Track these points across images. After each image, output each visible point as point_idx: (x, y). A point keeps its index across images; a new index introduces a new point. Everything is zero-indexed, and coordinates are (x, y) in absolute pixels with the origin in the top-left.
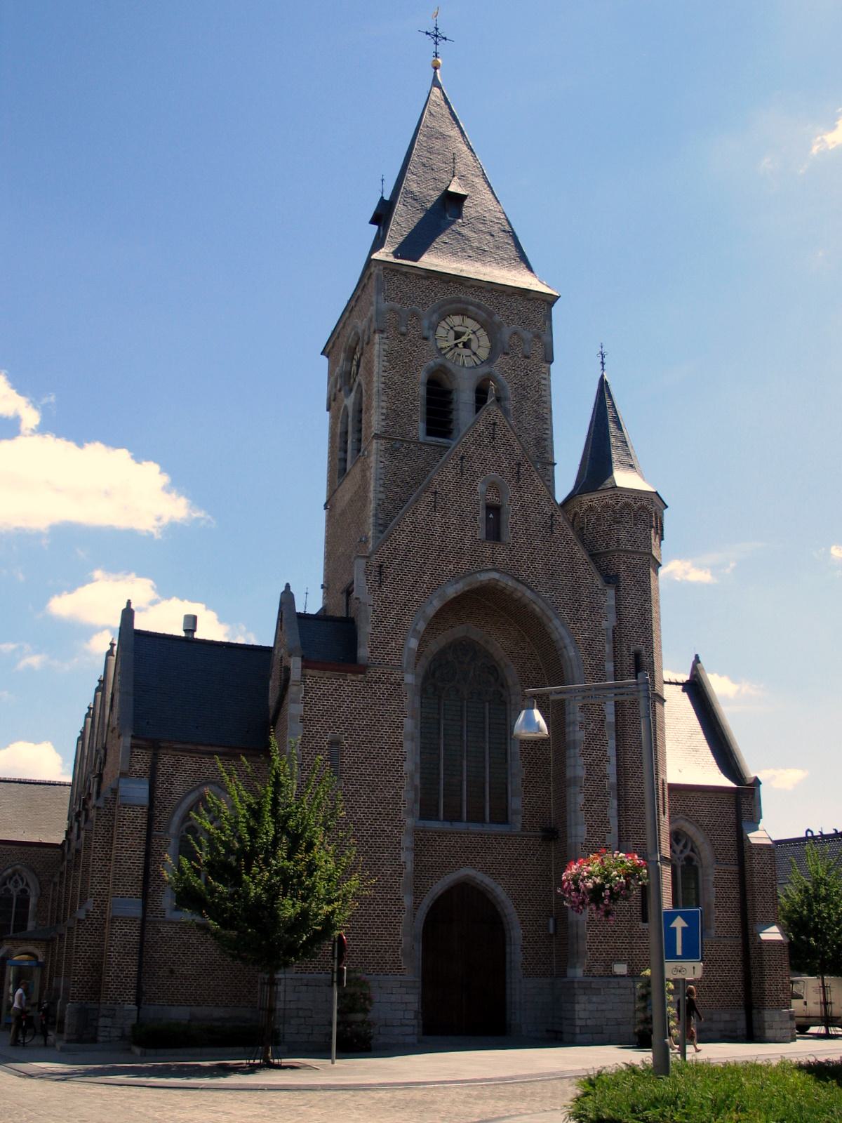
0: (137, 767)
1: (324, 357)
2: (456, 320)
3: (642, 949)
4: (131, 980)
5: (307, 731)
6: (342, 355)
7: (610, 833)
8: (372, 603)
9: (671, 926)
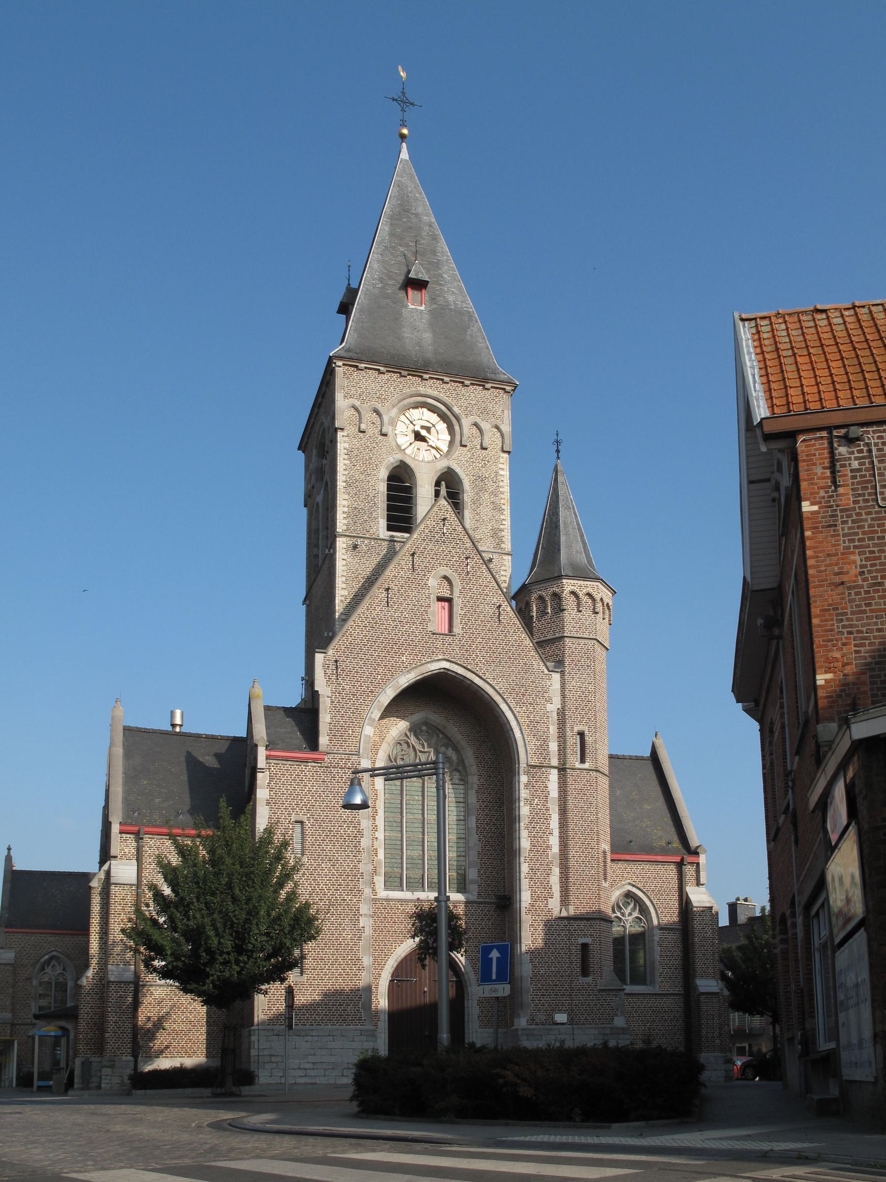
0: (126, 850)
1: (300, 452)
2: (415, 414)
3: (581, 1000)
4: (127, 1036)
5: (272, 813)
6: (314, 451)
7: (552, 898)
8: (330, 695)
9: (490, 956)
